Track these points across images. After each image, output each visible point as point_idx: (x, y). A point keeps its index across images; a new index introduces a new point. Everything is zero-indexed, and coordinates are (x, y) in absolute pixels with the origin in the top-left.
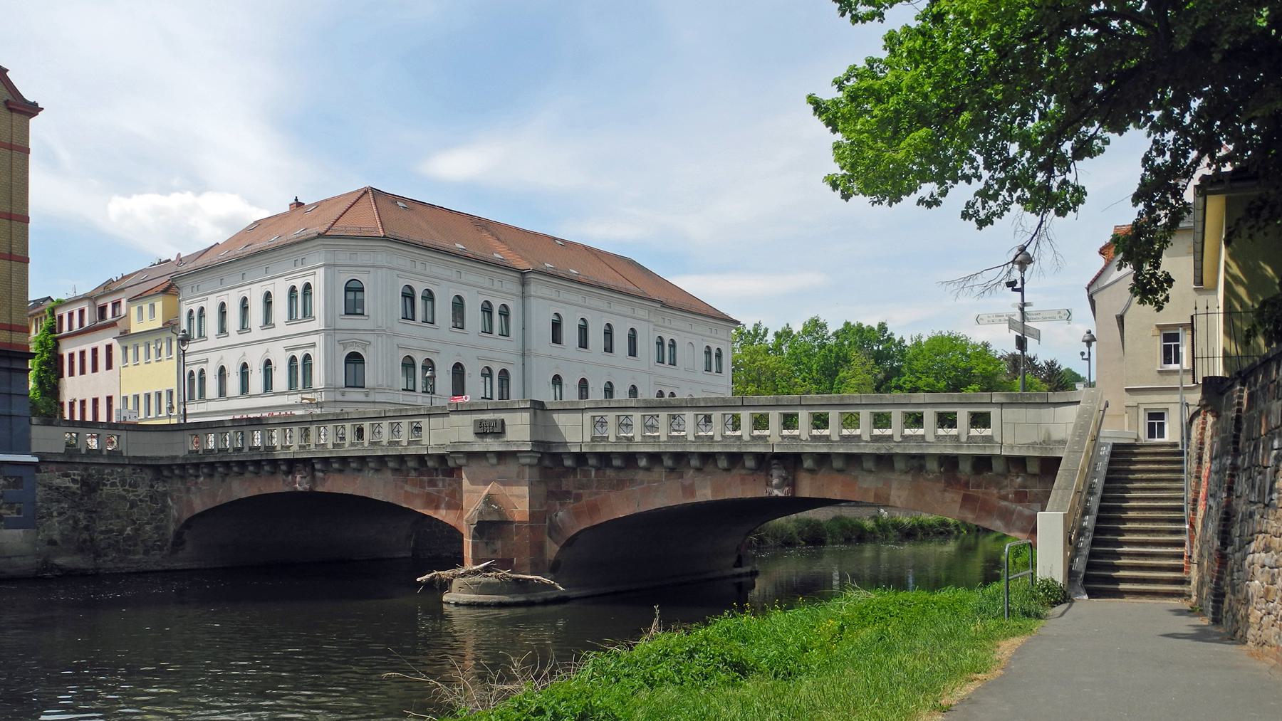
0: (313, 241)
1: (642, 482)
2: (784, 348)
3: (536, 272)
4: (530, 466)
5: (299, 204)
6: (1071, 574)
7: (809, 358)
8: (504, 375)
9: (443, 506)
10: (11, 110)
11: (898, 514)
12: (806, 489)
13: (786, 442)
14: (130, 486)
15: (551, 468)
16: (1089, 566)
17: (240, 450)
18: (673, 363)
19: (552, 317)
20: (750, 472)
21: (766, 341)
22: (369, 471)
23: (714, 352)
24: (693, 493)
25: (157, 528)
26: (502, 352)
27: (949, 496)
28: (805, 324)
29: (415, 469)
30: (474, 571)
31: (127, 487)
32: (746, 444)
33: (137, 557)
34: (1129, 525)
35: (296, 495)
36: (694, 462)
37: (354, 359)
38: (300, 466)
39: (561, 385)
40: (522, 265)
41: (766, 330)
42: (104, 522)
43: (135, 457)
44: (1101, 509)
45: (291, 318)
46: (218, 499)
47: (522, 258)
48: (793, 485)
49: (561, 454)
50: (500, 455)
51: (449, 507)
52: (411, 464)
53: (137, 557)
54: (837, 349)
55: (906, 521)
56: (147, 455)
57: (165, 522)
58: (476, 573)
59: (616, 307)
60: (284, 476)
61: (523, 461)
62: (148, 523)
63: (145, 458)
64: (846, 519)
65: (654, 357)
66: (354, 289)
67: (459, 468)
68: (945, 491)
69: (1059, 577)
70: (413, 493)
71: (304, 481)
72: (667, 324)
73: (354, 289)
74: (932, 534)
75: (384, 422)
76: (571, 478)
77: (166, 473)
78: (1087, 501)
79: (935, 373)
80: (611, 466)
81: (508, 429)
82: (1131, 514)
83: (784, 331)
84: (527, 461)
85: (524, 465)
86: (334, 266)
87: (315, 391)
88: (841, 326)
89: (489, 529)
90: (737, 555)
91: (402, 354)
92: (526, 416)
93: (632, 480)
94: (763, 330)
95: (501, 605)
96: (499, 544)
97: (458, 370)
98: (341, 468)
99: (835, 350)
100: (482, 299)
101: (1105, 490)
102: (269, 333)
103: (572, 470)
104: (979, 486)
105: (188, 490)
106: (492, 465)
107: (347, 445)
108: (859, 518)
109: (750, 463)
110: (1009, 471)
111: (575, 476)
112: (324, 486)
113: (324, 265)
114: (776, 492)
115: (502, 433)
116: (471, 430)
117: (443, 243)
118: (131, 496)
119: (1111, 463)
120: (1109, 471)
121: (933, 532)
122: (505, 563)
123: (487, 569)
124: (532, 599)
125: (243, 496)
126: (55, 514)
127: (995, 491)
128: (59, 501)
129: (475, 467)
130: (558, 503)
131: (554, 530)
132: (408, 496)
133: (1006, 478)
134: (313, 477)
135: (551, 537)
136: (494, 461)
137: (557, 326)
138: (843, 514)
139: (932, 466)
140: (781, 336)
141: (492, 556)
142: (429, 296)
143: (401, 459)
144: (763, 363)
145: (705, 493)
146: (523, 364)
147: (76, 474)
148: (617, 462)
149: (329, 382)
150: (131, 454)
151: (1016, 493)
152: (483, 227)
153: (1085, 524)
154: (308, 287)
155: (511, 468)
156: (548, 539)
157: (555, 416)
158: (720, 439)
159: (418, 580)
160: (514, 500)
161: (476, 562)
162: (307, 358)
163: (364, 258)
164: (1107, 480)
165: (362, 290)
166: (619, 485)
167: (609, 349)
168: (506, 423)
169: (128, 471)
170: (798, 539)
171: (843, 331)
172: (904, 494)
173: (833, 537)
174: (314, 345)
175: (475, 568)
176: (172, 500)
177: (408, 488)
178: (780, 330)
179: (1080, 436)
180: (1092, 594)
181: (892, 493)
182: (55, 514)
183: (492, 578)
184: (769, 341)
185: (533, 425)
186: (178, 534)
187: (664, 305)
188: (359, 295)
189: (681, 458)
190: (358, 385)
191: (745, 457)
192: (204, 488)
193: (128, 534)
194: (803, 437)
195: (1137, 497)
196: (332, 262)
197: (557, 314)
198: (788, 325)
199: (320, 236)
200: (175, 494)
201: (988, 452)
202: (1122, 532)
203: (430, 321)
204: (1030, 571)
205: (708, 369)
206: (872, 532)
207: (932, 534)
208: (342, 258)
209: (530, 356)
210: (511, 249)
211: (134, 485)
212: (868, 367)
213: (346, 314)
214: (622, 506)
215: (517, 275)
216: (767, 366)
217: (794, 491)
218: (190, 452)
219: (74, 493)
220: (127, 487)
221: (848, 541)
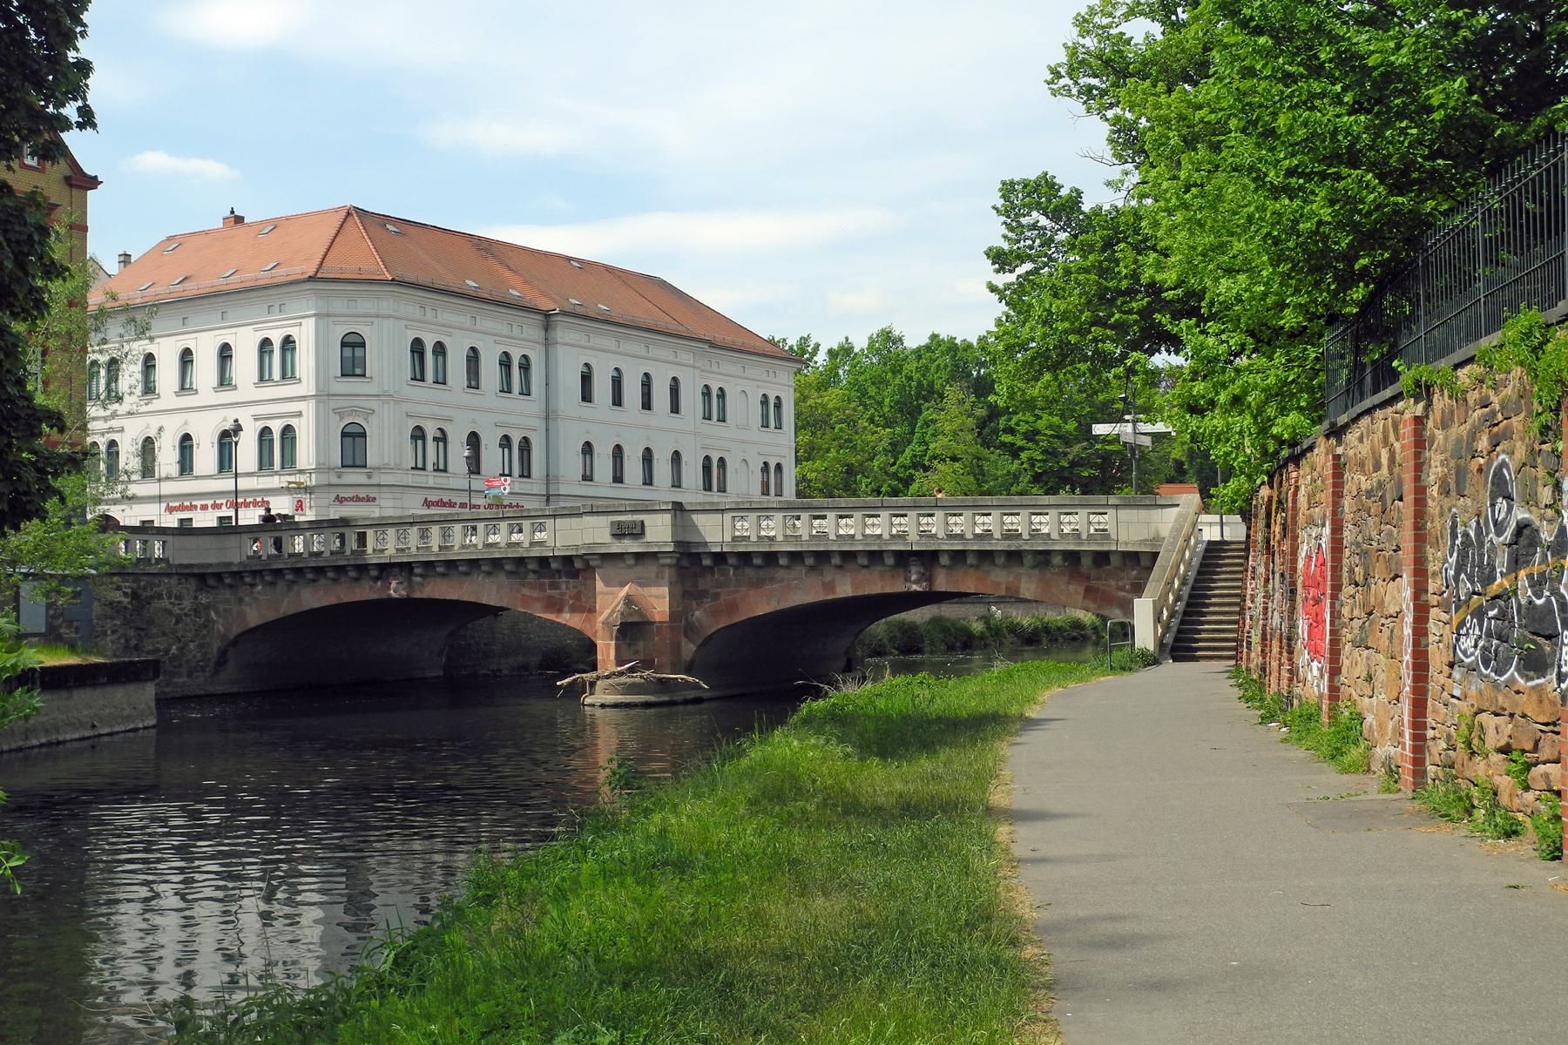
0: (300, 285)
1: (782, 580)
2: (841, 372)
3: (563, 313)
4: (670, 566)
5: (239, 220)
6: (1161, 645)
7: (878, 388)
8: (526, 445)
9: (567, 609)
10: (71, 186)
11: (1014, 614)
12: (942, 584)
13: (924, 540)
14: (176, 598)
16: (1176, 640)
17: (319, 554)
18: (722, 419)
19: (581, 368)
21: (816, 362)
23: (772, 401)
25: (201, 646)
26: (522, 415)
27: (1072, 588)
28: (871, 338)
29: (534, 572)
30: (619, 672)
31: (173, 600)
32: (886, 542)
33: (181, 680)
34: (1211, 609)
35: (391, 601)
36: (836, 560)
37: (354, 437)
38: (396, 570)
39: (591, 455)
40: (545, 305)
41: (817, 346)
42: (151, 640)
43: (181, 566)
44: (1191, 596)
45: (261, 379)
46: (282, 611)
47: (542, 293)
49: (699, 554)
50: (639, 556)
51: (574, 610)
52: (531, 566)
53: (181, 680)
54: (918, 375)
55: (1025, 622)
56: (192, 562)
57: (208, 638)
58: (621, 674)
59: (655, 352)
60: (371, 583)
62: (191, 641)
63: (192, 566)
64: (948, 620)
66: (353, 344)
67: (593, 569)
68: (1069, 583)
69: (1151, 647)
70: (531, 597)
71: (401, 587)
72: (714, 368)
73: (353, 344)
74: (1061, 640)
75: (501, 523)
76: (709, 578)
77: (211, 582)
78: (1181, 590)
79: (1060, 410)
81: (648, 530)
82: (1214, 600)
83: (842, 348)
84: (668, 561)
85: (663, 566)
86: (328, 315)
87: (301, 472)
88: (924, 341)
89: (631, 630)
90: (845, 659)
91: (412, 424)
92: (668, 517)
94: (812, 346)
95: (647, 705)
96: (641, 644)
97: (474, 440)
98: (514, 569)
99: (916, 376)
100: (500, 350)
101: (1196, 581)
102: (226, 396)
103: (710, 569)
104: (1099, 579)
105: (241, 600)
106: (629, 567)
107: (456, 548)
108: (964, 619)
109: (890, 561)
110: (1125, 565)
111: (713, 575)
112: (422, 592)
113: (315, 315)
114: (915, 587)
115: (642, 533)
116: (607, 531)
117: (452, 282)
119: (1204, 558)
120: (1202, 565)
121: (1064, 637)
122: (647, 664)
123: (631, 670)
124: (675, 698)
125: (317, 605)
126: (109, 632)
127: (1113, 583)
128: (112, 618)
129: (610, 569)
130: (694, 603)
132: (526, 600)
133: (1123, 571)
134: (410, 581)
135: (687, 637)
136: (632, 562)
137: (586, 379)
138: (943, 614)
139: (1057, 560)
140: (837, 354)
141: (634, 658)
142: (440, 349)
143: (520, 561)
144: (819, 401)
145: (845, 588)
146: (547, 430)
147: (128, 586)
149: (322, 461)
150: (176, 562)
151: (1132, 585)
152: (487, 250)
153: (1177, 608)
154: (288, 342)
155: (650, 569)
157: (694, 517)
158: (861, 538)
159: (558, 683)
160: (654, 601)
161: (620, 663)
162: (288, 431)
163: (366, 305)
164: (1199, 573)
165: (363, 345)
166: (758, 584)
167: (647, 405)
168: (646, 524)
169: (174, 581)
170: (889, 648)
171: (928, 348)
172: (1033, 587)
173: (932, 644)
174: (300, 414)
175: (619, 669)
176: (217, 613)
177: (526, 591)
178: (835, 347)
179: (1174, 538)
180: (1175, 659)
181: (1022, 586)
182: (109, 632)
183: (636, 678)
184: (820, 362)
185: (674, 525)
186: (223, 653)
187: (712, 345)
188: (358, 352)
189: (822, 557)
190: (358, 463)
191: (885, 555)
192: (261, 598)
194: (940, 536)
195: (1221, 586)
196: (324, 311)
197: (586, 365)
198: (847, 339)
199: (311, 279)
200: (221, 607)
201: (1105, 548)
202: (1204, 614)
203: (441, 380)
204: (1130, 642)
205: (765, 425)
206: (982, 637)
207: (1061, 640)
208: (338, 306)
209: (555, 420)
210: (526, 282)
211: (179, 598)
212: (967, 406)
213: (343, 375)
214: (762, 603)
216: (823, 406)
217: (930, 585)
218: (248, 557)
219: (126, 608)
220: (173, 600)
221: (951, 648)
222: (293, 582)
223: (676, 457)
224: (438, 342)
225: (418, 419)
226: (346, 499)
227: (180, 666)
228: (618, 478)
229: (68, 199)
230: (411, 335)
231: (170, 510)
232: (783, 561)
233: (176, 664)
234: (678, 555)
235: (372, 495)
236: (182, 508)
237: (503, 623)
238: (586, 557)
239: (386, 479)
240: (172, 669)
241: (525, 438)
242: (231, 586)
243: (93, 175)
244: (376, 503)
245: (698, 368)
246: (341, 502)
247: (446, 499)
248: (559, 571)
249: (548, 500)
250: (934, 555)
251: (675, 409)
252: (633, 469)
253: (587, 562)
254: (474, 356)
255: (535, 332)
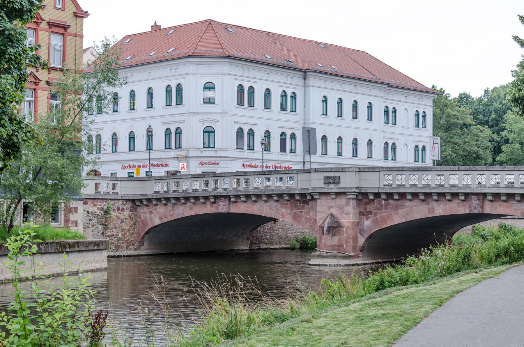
1: (408, 207)
4: (353, 199)
10: (76, 16)
12: (488, 209)
15: (362, 200)
18: (394, 123)
20: (461, 202)
22: (261, 202)
23: (391, 110)
24: (434, 213)
31: (120, 211)
37: (209, 132)
48: (482, 207)
50: (338, 194)
61: (349, 197)
65: (383, 120)
80: (393, 199)
84: (352, 196)
85: (349, 199)
91: (237, 127)
93: (403, 205)
98: (256, 200)
116: (323, 181)
118: (121, 217)
131: (362, 232)
135: (361, 234)
148: (396, 197)
150: (122, 194)
155: (342, 201)
156: (359, 235)
169: (121, 202)
187: (389, 85)
193: (120, 237)
205: (417, 126)
215: (302, 73)
217: (483, 210)
219: (98, 215)
222: (175, 204)
223: (370, 143)
224: (251, 86)
225: (394, 140)
226: (205, 164)
227: (123, 243)
228: (340, 154)
229: (75, 23)
230: (238, 83)
231: (124, 167)
232: (409, 197)
233: (121, 242)
234: (357, 194)
235: (217, 162)
236: (129, 167)
237: (278, 226)
238: (311, 194)
239: (224, 154)
240: (119, 244)
241: (251, 129)
242: (147, 206)
243: (86, 11)
244: (219, 165)
245: (382, 97)
246: (203, 165)
247: (253, 164)
248: (299, 200)
249: (304, 164)
250: (485, 195)
251: (370, 119)
252: (348, 149)
253: (312, 196)
254: (268, 93)
255: (300, 81)
